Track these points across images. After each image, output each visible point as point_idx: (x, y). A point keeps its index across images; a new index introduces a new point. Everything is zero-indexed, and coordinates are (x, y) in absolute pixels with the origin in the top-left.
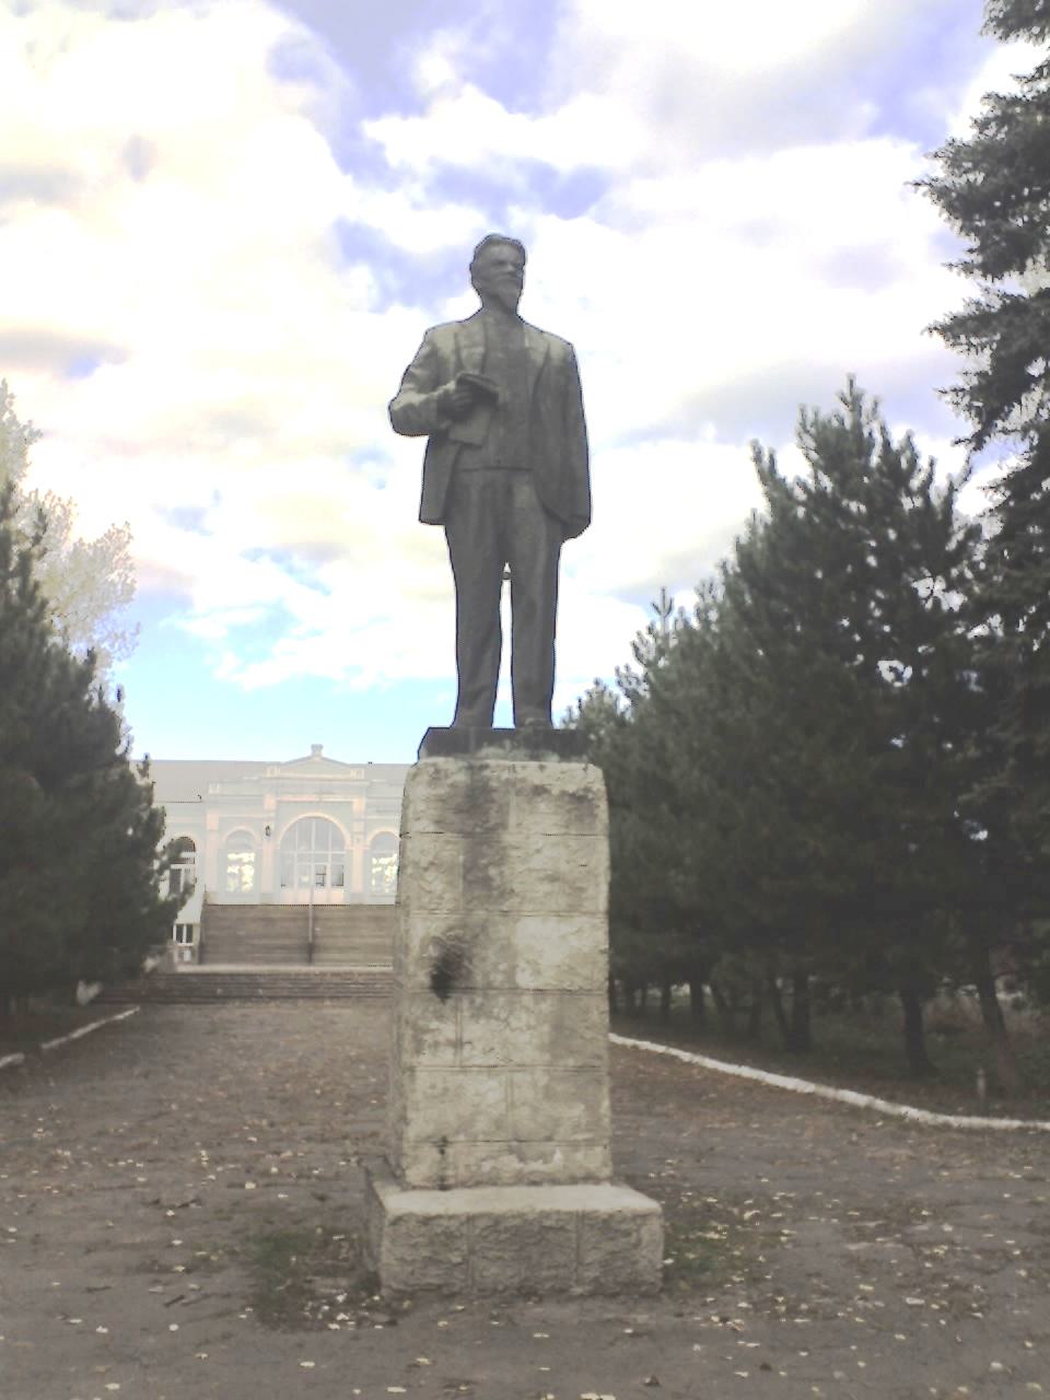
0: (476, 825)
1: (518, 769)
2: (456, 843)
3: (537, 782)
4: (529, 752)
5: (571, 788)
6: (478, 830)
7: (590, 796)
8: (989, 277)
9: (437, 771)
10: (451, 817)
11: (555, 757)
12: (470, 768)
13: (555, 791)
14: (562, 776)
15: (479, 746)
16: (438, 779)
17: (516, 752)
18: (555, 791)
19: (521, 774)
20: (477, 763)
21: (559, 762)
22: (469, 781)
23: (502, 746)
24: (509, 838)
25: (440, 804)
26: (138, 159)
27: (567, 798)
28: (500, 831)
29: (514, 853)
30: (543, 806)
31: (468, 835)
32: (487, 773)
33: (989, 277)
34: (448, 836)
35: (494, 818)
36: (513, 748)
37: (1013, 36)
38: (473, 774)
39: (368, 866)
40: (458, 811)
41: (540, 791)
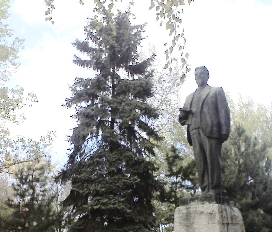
0: (188, 223)
1: (197, 208)
2: (184, 228)
3: (201, 210)
4: (201, 202)
5: (209, 211)
6: (188, 224)
7: (213, 213)
8: (138, 178)
9: (179, 210)
10: (183, 221)
11: (207, 203)
12: (187, 208)
13: (205, 213)
14: (207, 208)
15: (190, 202)
16: (180, 212)
17: (198, 203)
18: (205, 213)
19: (198, 209)
20: (188, 207)
21: (209, 204)
22: (186, 212)
23: (195, 202)
24: (195, 226)
25: (180, 218)
26: (132, 4)
27: (208, 214)
28: (193, 224)
29: (197, 230)
30: (203, 216)
31: (187, 226)
32: (190, 209)
33: (138, 178)
34: (182, 226)
35: (192, 221)
36: (198, 202)
37: (162, 137)
38: (187, 210)
39: (22, 209)
40: (185, 220)
41: (202, 213)
